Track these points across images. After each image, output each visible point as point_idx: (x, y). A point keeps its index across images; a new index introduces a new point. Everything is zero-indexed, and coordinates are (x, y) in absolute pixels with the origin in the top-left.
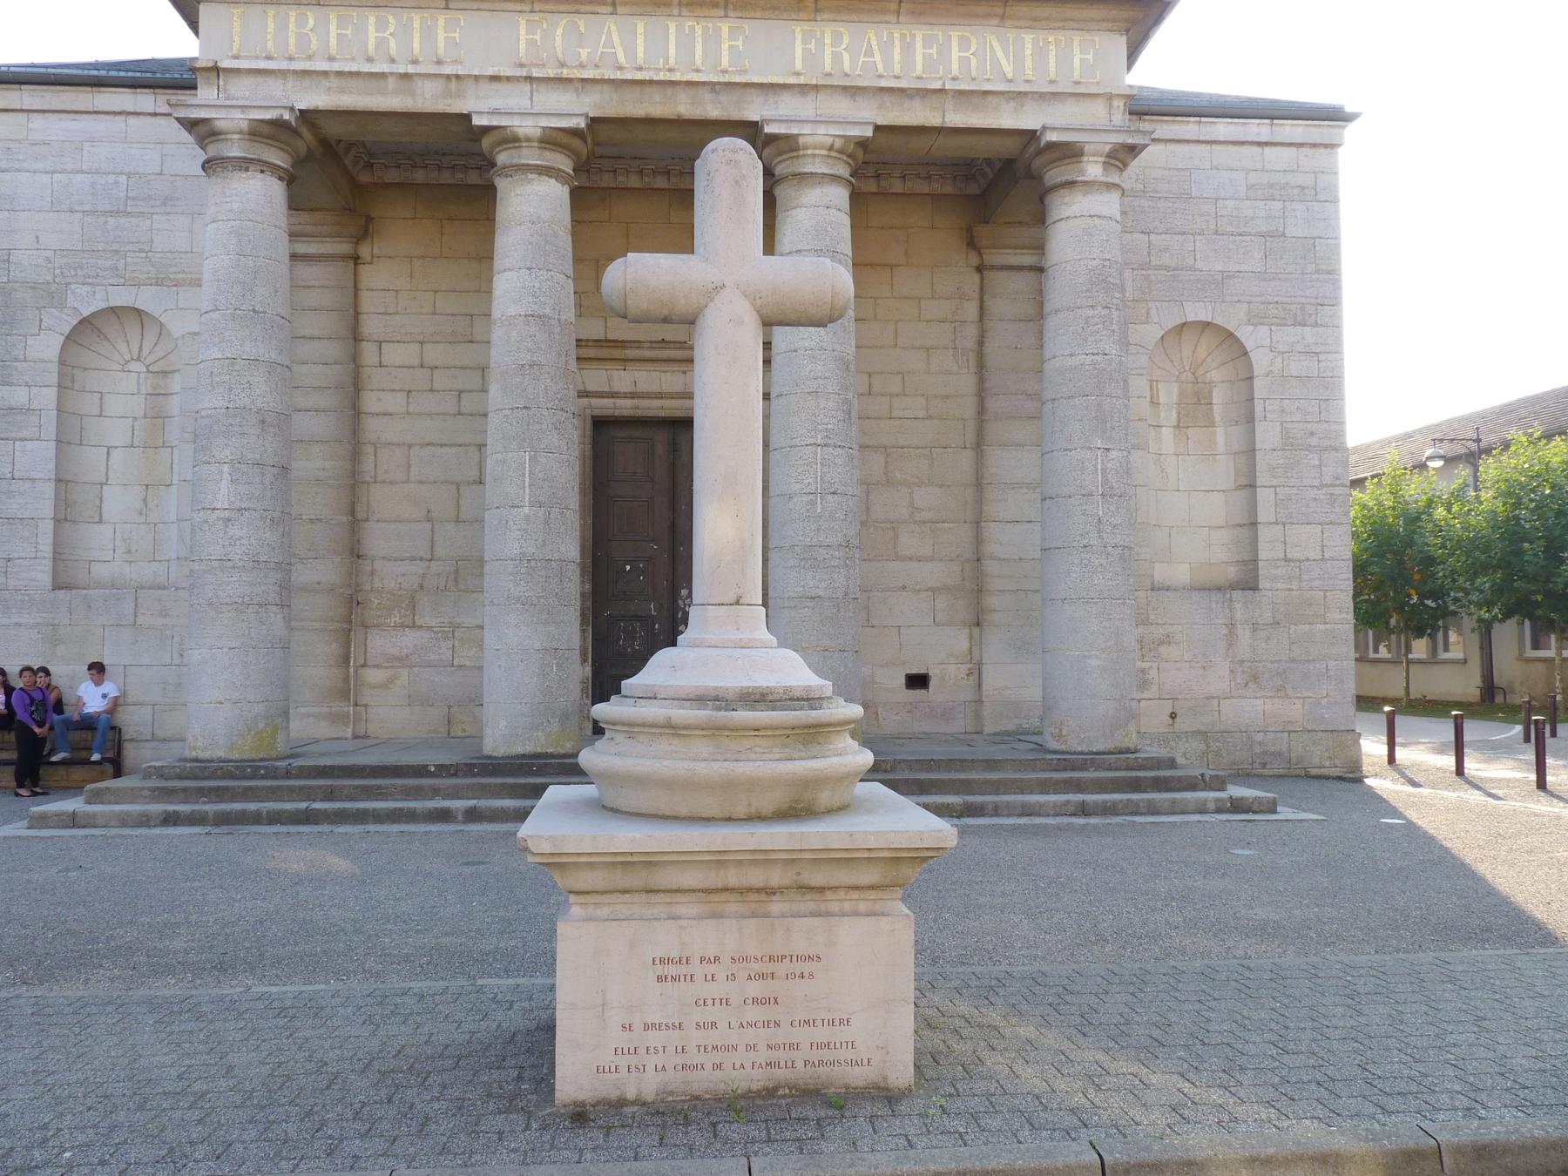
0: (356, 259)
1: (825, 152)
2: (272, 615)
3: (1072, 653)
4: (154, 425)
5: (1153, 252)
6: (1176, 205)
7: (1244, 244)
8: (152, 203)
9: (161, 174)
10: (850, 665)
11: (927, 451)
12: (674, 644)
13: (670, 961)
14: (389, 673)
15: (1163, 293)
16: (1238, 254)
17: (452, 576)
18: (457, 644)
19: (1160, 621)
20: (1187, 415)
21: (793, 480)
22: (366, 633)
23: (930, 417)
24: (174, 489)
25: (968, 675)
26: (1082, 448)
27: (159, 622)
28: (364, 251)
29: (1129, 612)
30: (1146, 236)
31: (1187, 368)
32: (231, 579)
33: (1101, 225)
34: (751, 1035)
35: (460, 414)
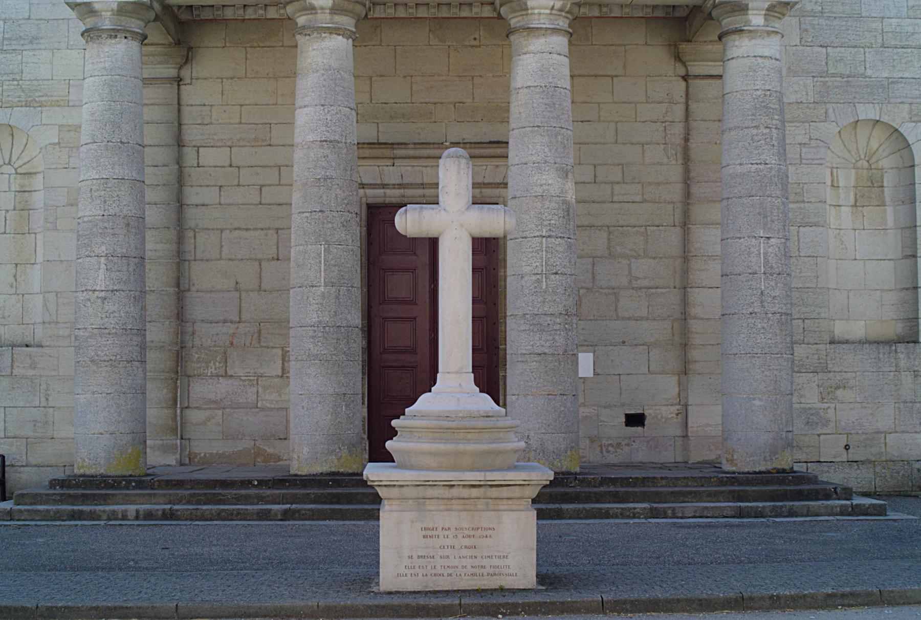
0: (179, 80)
1: (548, 11)
2: (135, 368)
3: (741, 396)
4: (21, 217)
5: (830, 62)
6: (849, 24)
7: (905, 55)
8: (22, 42)
9: (29, 19)
10: (569, 405)
11: (643, 229)
12: (430, 391)
13: (429, 529)
14: (208, 413)
15: (839, 96)
16: (901, 63)
17: (256, 335)
18: (260, 390)
19: (837, 369)
20: (862, 196)
21: (524, 264)
22: (189, 381)
23: (644, 201)
24: (37, 267)
25: (677, 415)
26: (749, 237)
27: (30, 373)
28: (186, 73)
29: (785, 364)
30: (824, 50)
31: (863, 157)
32: (108, 343)
33: (763, 63)
34: (464, 562)
35: (261, 204)
